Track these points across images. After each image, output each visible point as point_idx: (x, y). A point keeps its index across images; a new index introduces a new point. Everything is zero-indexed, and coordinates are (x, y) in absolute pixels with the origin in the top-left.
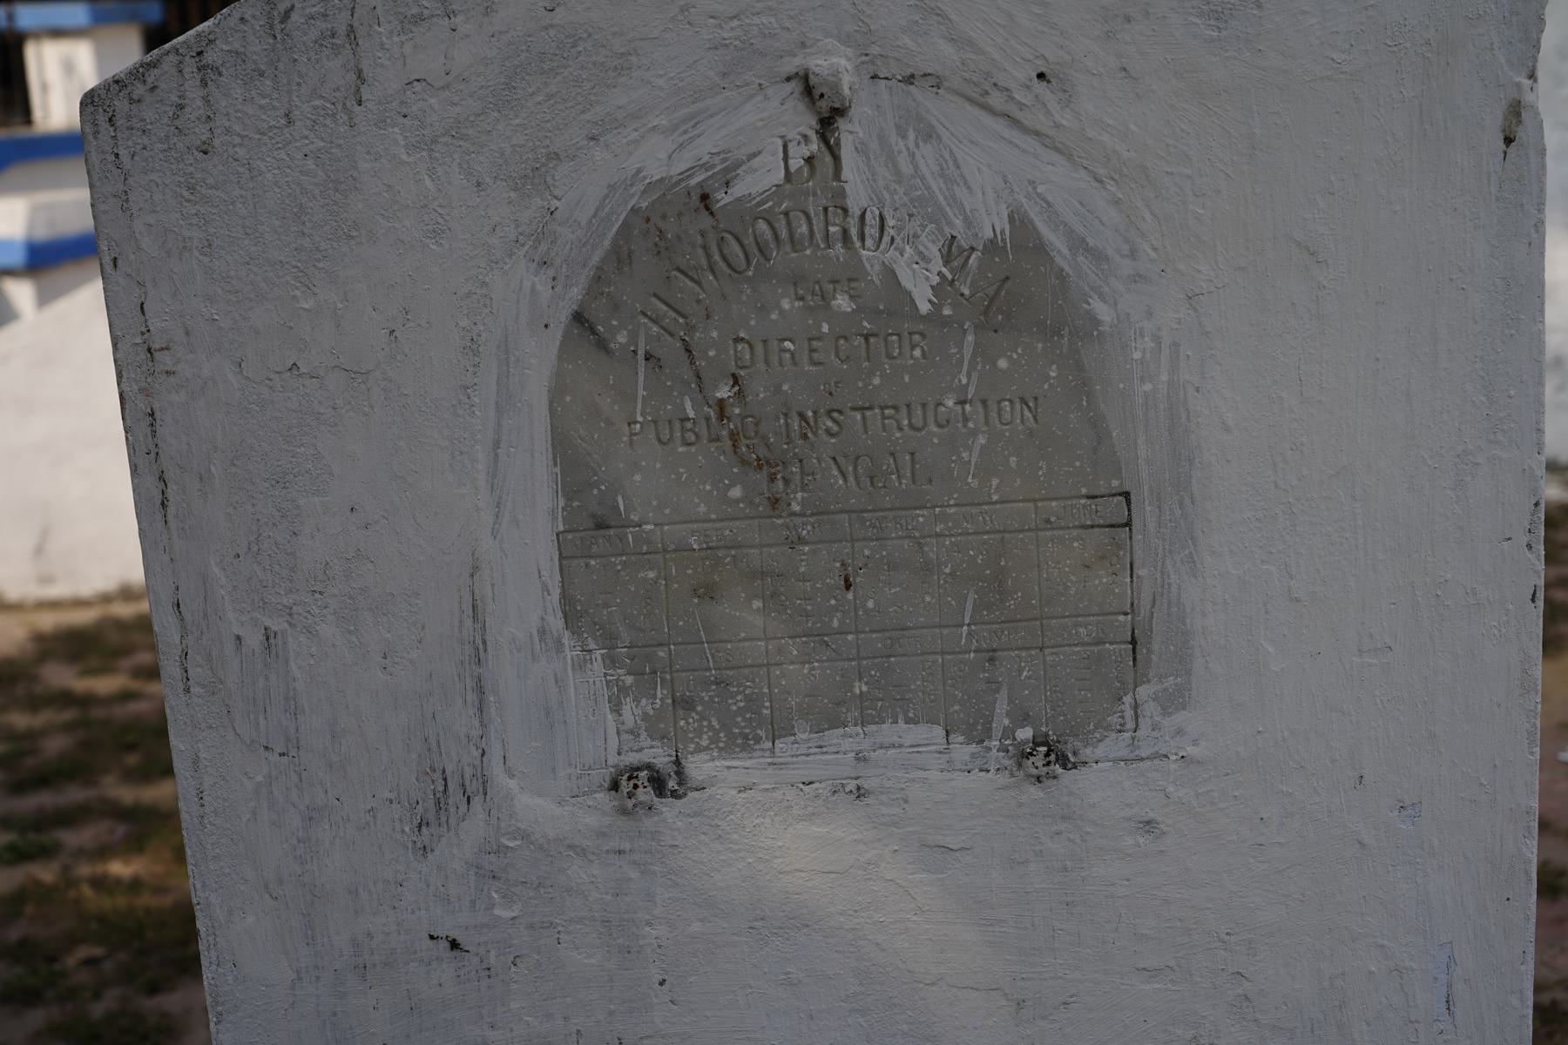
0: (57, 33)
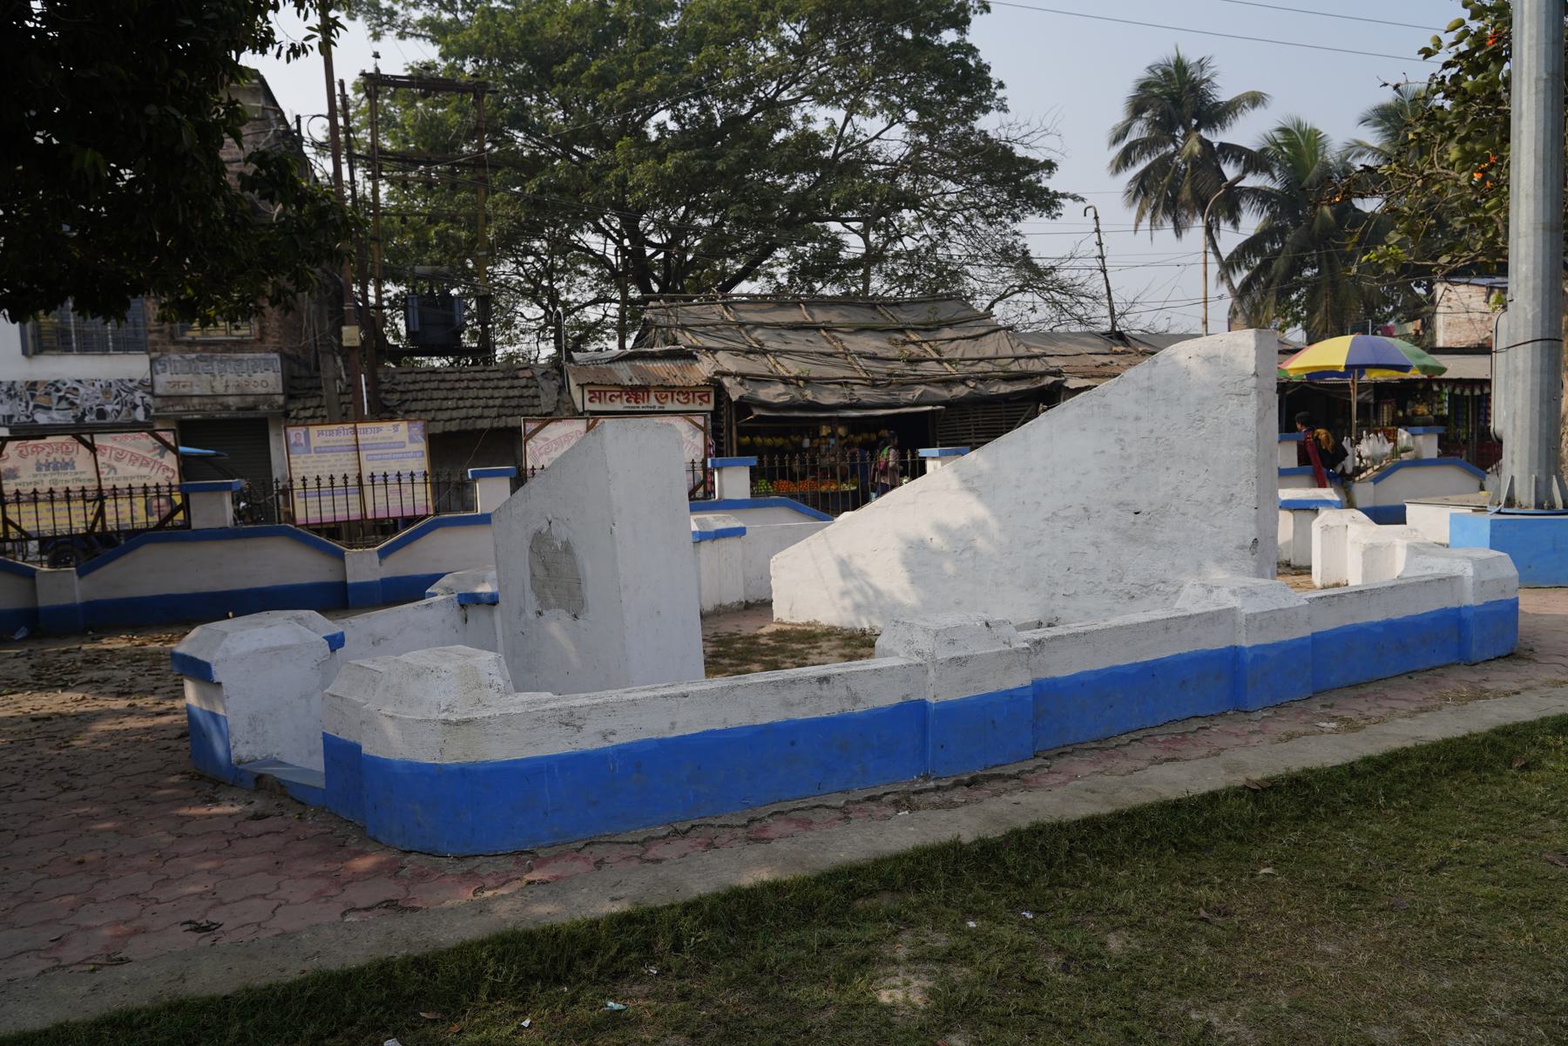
0: (934, 458)
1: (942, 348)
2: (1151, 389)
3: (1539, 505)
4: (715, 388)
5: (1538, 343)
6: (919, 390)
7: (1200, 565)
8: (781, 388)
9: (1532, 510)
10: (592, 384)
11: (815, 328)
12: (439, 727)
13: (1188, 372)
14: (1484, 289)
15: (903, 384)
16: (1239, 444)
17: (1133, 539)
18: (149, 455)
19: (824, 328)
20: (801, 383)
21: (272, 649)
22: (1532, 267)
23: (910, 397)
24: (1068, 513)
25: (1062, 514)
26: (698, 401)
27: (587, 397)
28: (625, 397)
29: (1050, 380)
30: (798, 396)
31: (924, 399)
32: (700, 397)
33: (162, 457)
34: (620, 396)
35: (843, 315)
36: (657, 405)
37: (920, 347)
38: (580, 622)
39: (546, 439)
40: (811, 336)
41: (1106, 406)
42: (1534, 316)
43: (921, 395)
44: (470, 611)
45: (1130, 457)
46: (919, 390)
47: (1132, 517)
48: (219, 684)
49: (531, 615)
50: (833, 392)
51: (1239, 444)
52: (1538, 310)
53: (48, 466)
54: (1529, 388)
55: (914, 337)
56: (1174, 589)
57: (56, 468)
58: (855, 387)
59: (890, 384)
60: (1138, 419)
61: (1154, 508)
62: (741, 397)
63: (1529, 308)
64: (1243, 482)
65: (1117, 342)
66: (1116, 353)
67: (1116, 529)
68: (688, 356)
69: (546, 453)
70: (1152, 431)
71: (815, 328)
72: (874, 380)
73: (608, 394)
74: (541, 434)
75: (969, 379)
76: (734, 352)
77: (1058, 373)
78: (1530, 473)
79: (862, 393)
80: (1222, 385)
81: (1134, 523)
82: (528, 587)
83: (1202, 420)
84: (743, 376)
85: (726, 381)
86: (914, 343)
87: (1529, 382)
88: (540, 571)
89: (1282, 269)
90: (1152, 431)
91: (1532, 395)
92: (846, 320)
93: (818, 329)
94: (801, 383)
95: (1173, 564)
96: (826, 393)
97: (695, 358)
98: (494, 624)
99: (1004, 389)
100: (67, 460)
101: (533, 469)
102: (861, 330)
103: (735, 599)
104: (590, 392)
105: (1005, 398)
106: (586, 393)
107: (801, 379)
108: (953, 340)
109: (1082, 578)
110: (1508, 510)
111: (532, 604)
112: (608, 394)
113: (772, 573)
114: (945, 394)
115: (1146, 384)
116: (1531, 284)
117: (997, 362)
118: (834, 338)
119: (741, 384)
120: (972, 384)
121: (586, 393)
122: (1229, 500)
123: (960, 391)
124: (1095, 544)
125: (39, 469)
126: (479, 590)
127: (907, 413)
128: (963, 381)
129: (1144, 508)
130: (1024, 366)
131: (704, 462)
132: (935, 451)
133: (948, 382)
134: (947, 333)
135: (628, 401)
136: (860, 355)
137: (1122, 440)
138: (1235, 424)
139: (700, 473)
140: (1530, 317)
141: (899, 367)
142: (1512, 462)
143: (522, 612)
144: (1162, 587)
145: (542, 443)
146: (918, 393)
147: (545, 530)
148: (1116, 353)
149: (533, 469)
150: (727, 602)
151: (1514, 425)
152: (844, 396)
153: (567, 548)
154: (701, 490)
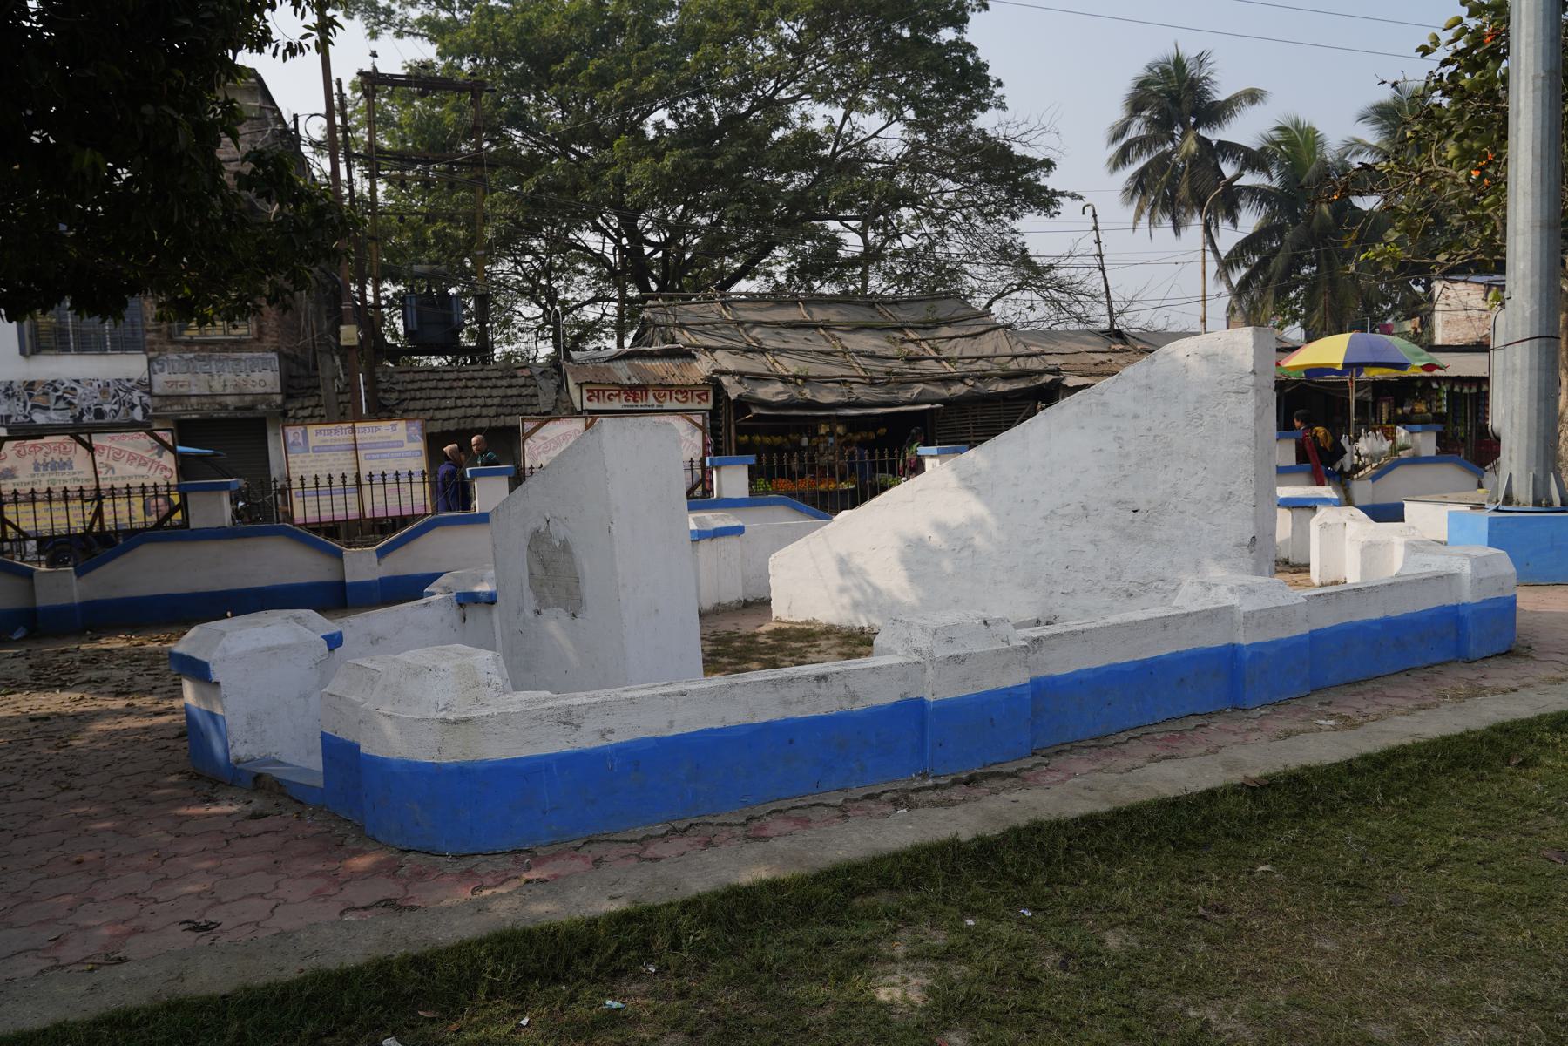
0: (932, 456)
1: (941, 346)
2: (1149, 387)
3: (1537, 503)
4: (714, 387)
5: (1537, 341)
6: (917, 389)
7: (1198, 563)
8: (779, 387)
9: (1530, 508)
10: (591, 383)
11: (814, 326)
12: (437, 725)
13: (1186, 369)
14: (1483, 287)
15: (901, 383)
16: (1237, 442)
17: (1131, 537)
18: (147, 455)
19: (822, 327)
20: (800, 382)
21: (270, 649)
22: (1529, 264)
23: (909, 395)
24: (1067, 510)
25: (1060, 512)
26: (697, 400)
27: (585, 395)
28: (623, 396)
29: (1048, 378)
30: (796, 395)
31: (922, 398)
32: (699, 396)
33: (160, 457)
34: (619, 395)
35: (842, 314)
36: (656, 403)
37: (919, 345)
38: (578, 620)
39: (544, 438)
40: (809, 334)
41: (1105, 404)
42: (1532, 313)
43: (920, 394)
44: (468, 610)
45: (1127, 455)
46: (917, 389)
47: (1130, 515)
48: (217, 683)
49: (529, 614)
50: (832, 391)
51: (1237, 442)
52: (1536, 307)
53: (45, 466)
54: (1526, 386)
55: (913, 336)
56: (1173, 587)
57: (53, 468)
58: (854, 386)
59: (888, 382)
60: (1136, 417)
61: (1152, 506)
62: (739, 396)
63: (1527, 306)
64: (1241, 480)
65: (1115, 340)
66: (1115, 351)
67: (1113, 527)
68: (687, 354)
69: (545, 452)
70: (1150, 429)
71: (814, 326)
72: (872, 379)
73: (607, 393)
74: (540, 433)
75: (968, 377)
76: (733, 351)
77: (1057, 371)
78: (1528, 470)
79: (860, 392)
80: (1220, 383)
81: (1133, 521)
82: (526, 585)
83: (1201, 417)
84: (742, 375)
85: (725, 380)
86: (912, 341)
87: (1527, 380)
88: (538, 570)
89: (1280, 268)
90: (1150, 429)
91: (1530, 392)
92: (845, 319)
93: (816, 328)
94: (800, 382)
95: (1172, 562)
96: (824, 392)
97: (694, 357)
98: (492, 623)
99: (1003, 387)
100: (65, 459)
101: (531, 468)
102: (859, 328)
103: (734, 598)
104: (588, 391)
105: (1004, 396)
106: (584, 392)
107: (800, 377)
108: (951, 338)
109: (1081, 575)
110: (1505, 508)
111: (530, 603)
112: (607, 393)
113: (770, 572)
114: (944, 392)
115: (1144, 382)
116: (1528, 282)
117: (996, 360)
118: (832, 336)
119: (740, 383)
120: (970, 383)
121: (584, 392)
122: (1227, 498)
123: (959, 389)
124: (1093, 542)
125: (37, 469)
126: (478, 589)
127: (905, 412)
128: (961, 380)
129: (1141, 506)
130: (1034, 364)
131: (703, 461)
132: (933, 450)
133: (946, 381)
134: (945, 331)
135: (626, 399)
136: (859, 353)
137: (1119, 438)
138: (1233, 422)
139: (699, 472)
140: (1527, 314)
141: (897, 366)
142: (1510, 459)
143: (520, 610)
144: (1161, 584)
145: (542, 442)
146: (916, 392)
147: (543, 529)
148: (1115, 351)
149: (531, 468)
150: (725, 601)
151: (1512, 423)
152: (843, 394)
153: (566, 547)
154: (700, 488)
